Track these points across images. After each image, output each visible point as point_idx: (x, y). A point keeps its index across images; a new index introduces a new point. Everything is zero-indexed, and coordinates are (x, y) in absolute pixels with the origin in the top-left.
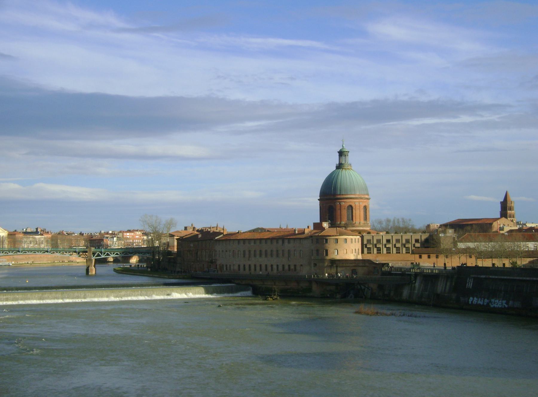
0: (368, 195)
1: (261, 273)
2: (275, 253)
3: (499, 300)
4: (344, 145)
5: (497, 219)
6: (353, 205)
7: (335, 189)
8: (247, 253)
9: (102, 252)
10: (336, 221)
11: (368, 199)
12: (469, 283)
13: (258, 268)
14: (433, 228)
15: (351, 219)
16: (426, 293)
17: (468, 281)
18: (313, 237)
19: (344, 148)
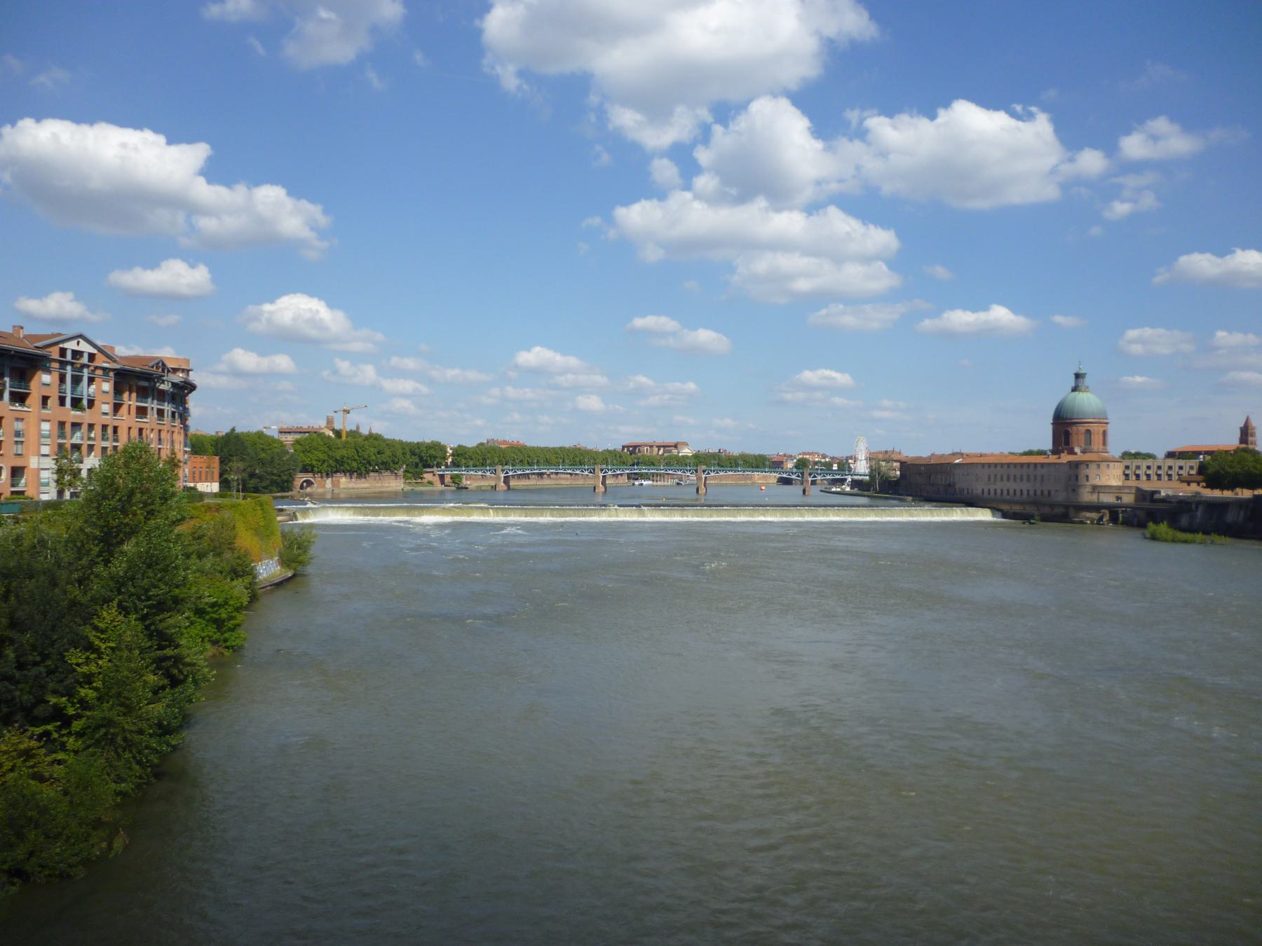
0: (1106, 419)
1: (1008, 497)
5: (186, 428)
6: (1091, 429)
8: (992, 477)
11: (1107, 423)
13: (1005, 492)
14: (493, 445)
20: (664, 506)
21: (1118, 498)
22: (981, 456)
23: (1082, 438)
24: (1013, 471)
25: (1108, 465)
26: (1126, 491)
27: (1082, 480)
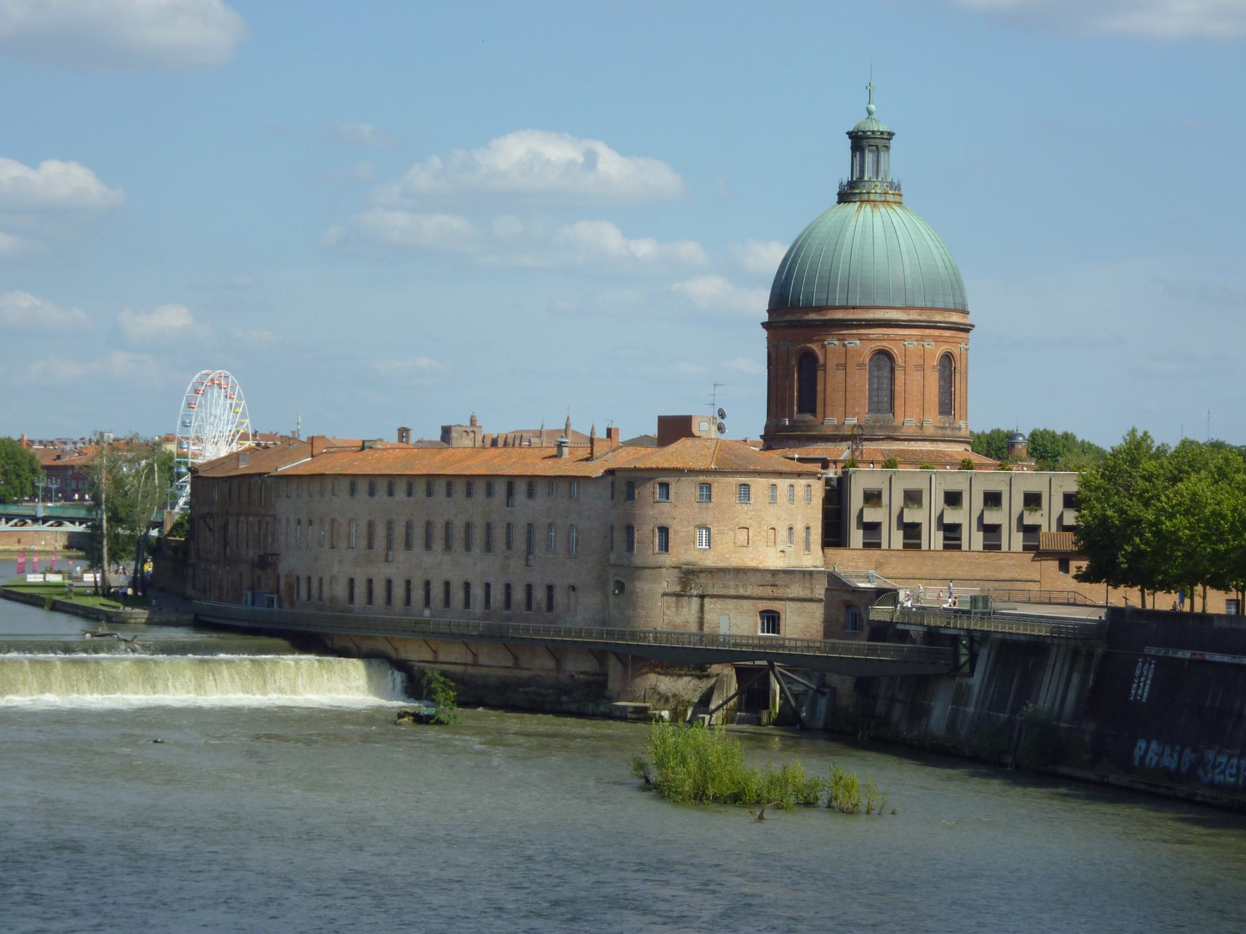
0: (965, 312)
2: (478, 535)
3: (1230, 757)
6: (896, 351)
8: (380, 531)
11: (966, 329)
12: (1139, 682)
13: (418, 594)
15: (887, 406)
16: (1002, 715)
17: (1138, 672)
18: (617, 474)
20: (45, 651)
21: (772, 620)
22: (363, 448)
23: (860, 381)
24: (446, 509)
26: (796, 590)
27: (647, 550)
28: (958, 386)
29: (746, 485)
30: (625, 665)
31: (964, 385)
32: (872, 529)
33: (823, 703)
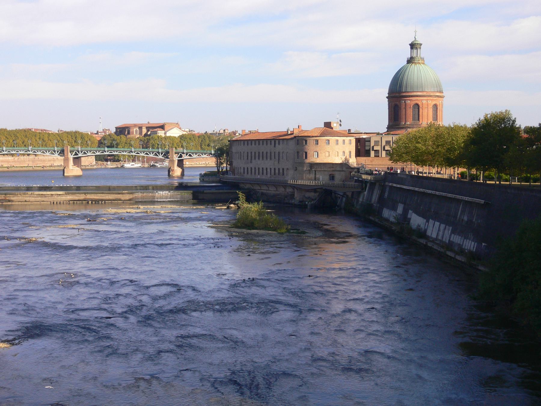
0: (441, 92)
4: (416, 37)
6: (420, 104)
7: (401, 86)
9: (159, 153)
10: (400, 122)
15: (417, 118)
19: (416, 39)
25: (329, 140)
28: (438, 113)
29: (329, 140)
30: (297, 190)
31: (441, 112)
32: (377, 151)
33: (344, 199)
